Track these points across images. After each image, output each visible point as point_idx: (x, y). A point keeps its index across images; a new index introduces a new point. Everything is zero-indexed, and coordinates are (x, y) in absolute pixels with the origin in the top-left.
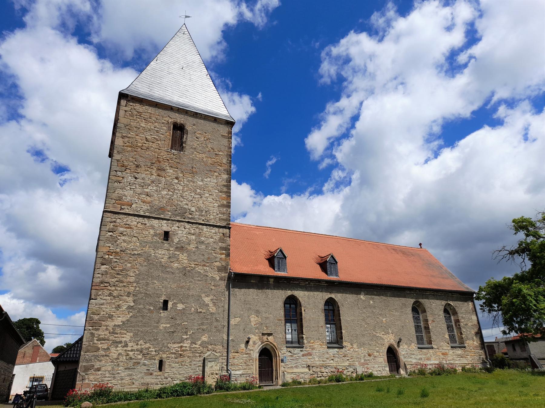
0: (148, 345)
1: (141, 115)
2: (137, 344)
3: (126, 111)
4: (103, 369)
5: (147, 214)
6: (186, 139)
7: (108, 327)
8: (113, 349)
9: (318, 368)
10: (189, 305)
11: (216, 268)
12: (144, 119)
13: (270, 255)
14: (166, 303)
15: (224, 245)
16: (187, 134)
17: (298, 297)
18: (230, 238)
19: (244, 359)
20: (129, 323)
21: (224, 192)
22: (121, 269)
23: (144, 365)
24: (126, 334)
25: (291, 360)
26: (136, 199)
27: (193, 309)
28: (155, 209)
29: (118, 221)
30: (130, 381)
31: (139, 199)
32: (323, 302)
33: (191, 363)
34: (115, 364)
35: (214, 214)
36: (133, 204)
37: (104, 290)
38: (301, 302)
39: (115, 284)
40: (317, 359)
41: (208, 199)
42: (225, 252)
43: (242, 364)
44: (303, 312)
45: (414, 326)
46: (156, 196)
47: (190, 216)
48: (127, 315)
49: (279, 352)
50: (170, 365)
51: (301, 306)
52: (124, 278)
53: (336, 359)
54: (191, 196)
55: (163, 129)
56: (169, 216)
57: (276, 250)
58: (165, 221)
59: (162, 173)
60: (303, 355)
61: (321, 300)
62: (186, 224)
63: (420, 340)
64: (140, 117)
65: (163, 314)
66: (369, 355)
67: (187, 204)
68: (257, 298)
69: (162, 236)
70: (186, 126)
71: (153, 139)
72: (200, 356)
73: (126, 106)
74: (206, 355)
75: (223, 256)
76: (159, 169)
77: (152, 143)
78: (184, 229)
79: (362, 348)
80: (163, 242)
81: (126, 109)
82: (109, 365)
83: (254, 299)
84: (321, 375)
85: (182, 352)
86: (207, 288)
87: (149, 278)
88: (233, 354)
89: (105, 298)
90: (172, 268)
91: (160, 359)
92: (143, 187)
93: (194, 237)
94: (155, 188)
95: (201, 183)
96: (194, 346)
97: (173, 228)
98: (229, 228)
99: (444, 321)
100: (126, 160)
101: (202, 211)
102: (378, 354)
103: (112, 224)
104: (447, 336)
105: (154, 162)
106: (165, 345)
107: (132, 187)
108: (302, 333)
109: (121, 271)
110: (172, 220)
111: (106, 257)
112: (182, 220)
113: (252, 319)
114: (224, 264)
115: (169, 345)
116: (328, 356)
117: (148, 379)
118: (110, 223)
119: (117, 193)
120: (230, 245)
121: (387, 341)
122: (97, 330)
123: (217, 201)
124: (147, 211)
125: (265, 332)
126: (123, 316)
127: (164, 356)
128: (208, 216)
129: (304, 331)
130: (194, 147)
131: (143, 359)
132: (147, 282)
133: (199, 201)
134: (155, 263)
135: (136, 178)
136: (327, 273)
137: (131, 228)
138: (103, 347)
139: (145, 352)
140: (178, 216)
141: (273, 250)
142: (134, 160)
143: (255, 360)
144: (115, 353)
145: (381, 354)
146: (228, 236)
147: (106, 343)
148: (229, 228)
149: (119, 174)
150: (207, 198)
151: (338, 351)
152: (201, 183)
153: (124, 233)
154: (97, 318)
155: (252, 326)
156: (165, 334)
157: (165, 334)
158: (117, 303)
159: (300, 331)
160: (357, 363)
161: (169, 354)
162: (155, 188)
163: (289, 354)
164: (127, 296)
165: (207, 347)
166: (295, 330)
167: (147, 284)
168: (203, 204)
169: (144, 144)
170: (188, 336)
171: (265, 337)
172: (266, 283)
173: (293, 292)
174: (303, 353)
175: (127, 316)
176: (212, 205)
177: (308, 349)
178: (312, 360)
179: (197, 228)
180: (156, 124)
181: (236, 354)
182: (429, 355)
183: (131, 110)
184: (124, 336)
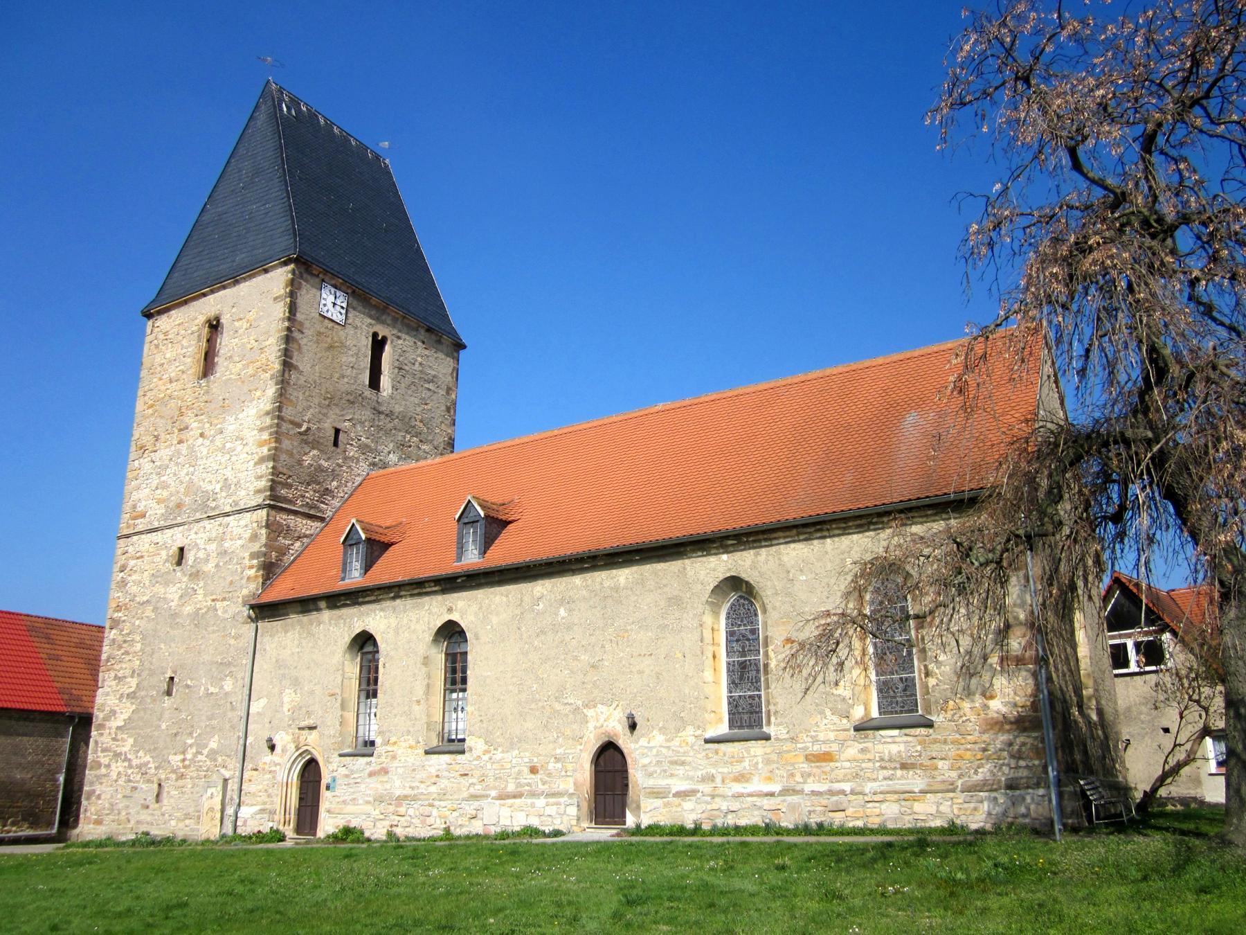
60: (371, 774)
66: (533, 770)
102: (559, 765)
181: (255, 773)
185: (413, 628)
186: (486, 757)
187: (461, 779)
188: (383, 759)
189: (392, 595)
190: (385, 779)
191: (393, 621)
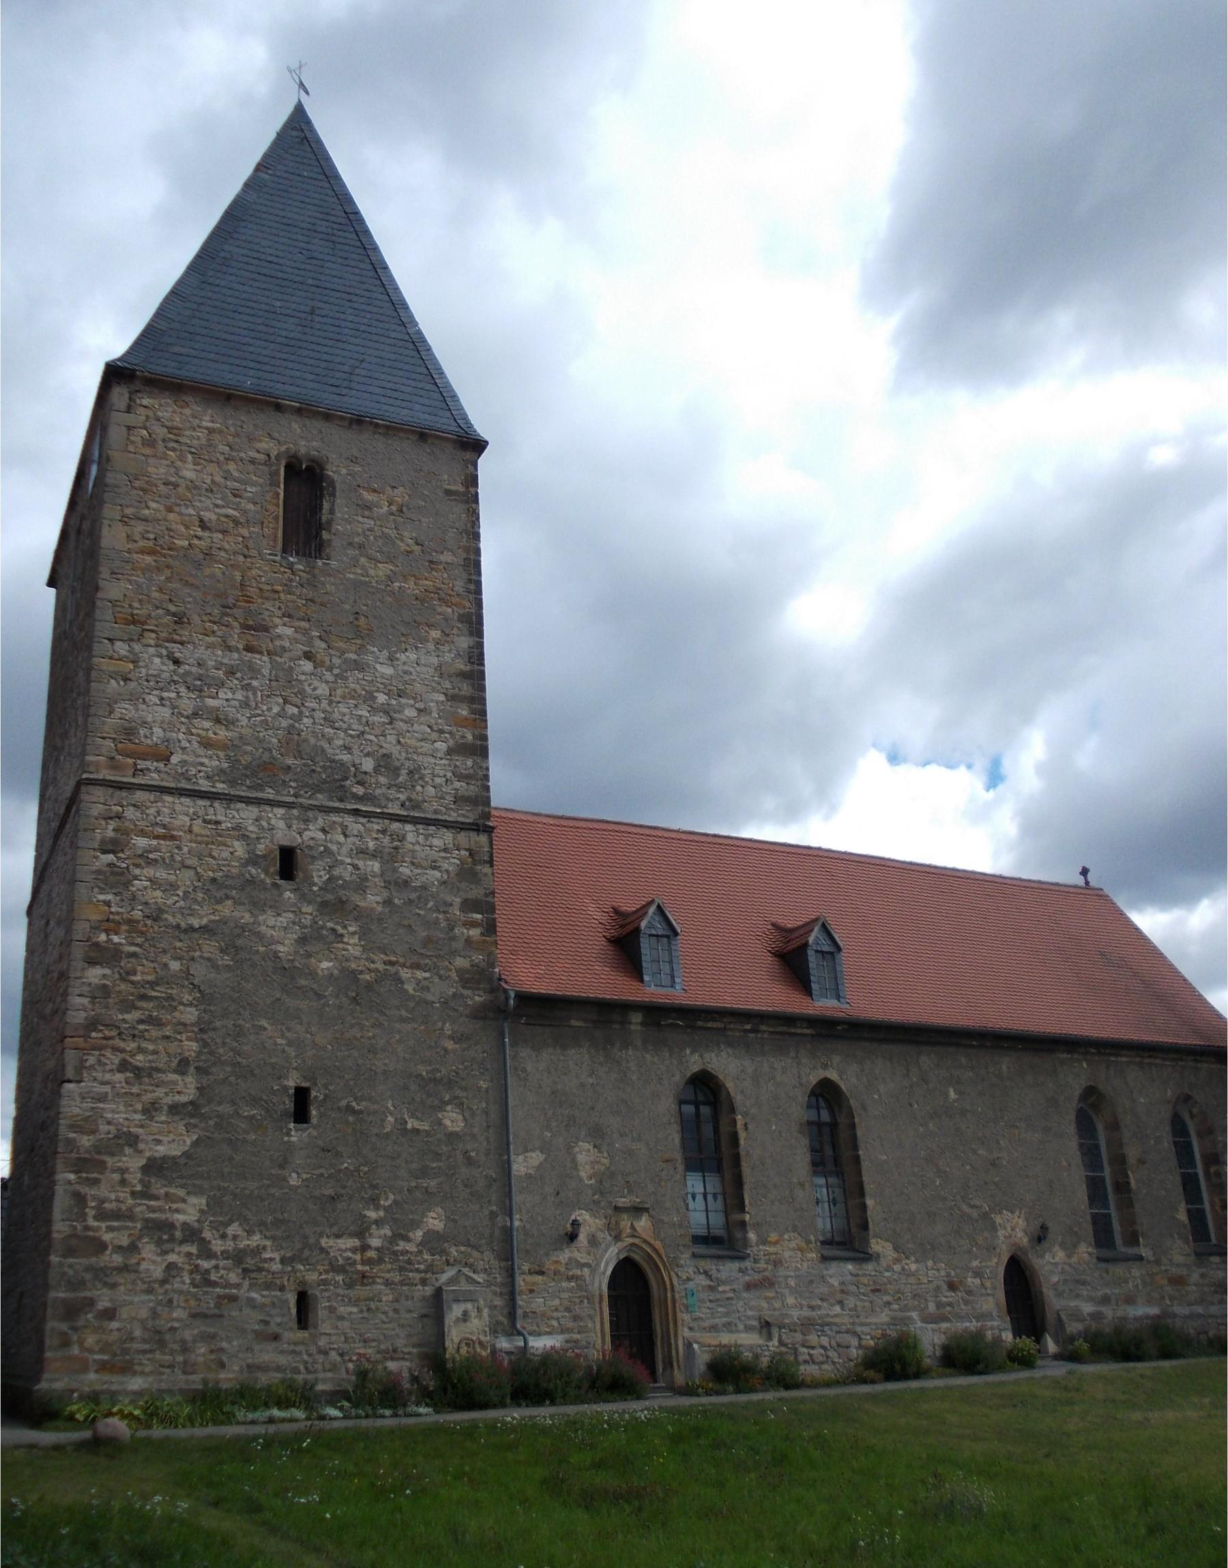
0: (256, 1240)
1: (181, 439)
2: (223, 1236)
3: (129, 428)
4: (124, 1313)
5: (220, 787)
6: (332, 512)
7: (126, 1176)
8: (148, 1250)
9: (795, 1331)
10: (376, 1107)
11: (454, 975)
12: (191, 453)
13: (622, 926)
14: (302, 1096)
15: (476, 892)
16: (333, 495)
17: (721, 1077)
18: (492, 866)
19: (563, 1295)
20: (191, 1163)
21: (465, 697)
22: (149, 978)
23: (251, 1303)
24: (184, 1201)
25: (710, 1301)
26: (181, 736)
27: (390, 1119)
28: (246, 768)
29: (130, 813)
30: (213, 1357)
31: (192, 734)
32: (802, 1097)
33: (396, 1305)
34: (160, 1298)
35: (438, 780)
36: (172, 753)
37: (103, 1052)
38: (732, 1094)
39: (136, 1032)
40: (790, 1300)
41: (416, 727)
42: (479, 916)
43: (560, 1314)
44: (742, 1135)
45: (1084, 1179)
46: (244, 722)
47: (359, 790)
48: (182, 1135)
49: (672, 1273)
50: (332, 1310)
51: (732, 1110)
52: (163, 1012)
53: (851, 1302)
54: (360, 716)
55: (253, 484)
56: (292, 792)
57: (644, 907)
58: (280, 811)
59: (264, 642)
60: (749, 1287)
61: (794, 1087)
62: (349, 820)
63: (1103, 1236)
64: (175, 445)
65: (296, 1135)
66: (952, 1287)
67: (347, 748)
68: (591, 1081)
69: (275, 865)
70: (328, 467)
71: (223, 519)
72: (424, 1282)
73: (129, 410)
74: (444, 1278)
75: (475, 933)
76: (249, 627)
77: (220, 536)
78: (341, 838)
79: (930, 1263)
80: (275, 885)
81: (131, 419)
82: (143, 1302)
83: (582, 1085)
84: (807, 1358)
85: (367, 1268)
86: (430, 1047)
87: (242, 1012)
88: (529, 1278)
89: (108, 1076)
90: (312, 974)
91: (300, 1289)
92: (201, 691)
93: (376, 866)
94: (240, 695)
95: (388, 671)
96: (402, 1245)
97: (307, 833)
98: (489, 830)
99: (1174, 1162)
100: (140, 601)
101: (396, 771)
102: (977, 1281)
103: (112, 825)
104: (1182, 1216)
105: (231, 601)
106: (312, 1241)
107: (165, 694)
108: (741, 1208)
109: (153, 985)
110: (302, 806)
111: (100, 939)
112: (331, 804)
113: (581, 1158)
114: (479, 958)
115: (324, 1242)
116: (824, 1289)
117: (267, 1354)
118: (103, 822)
119: (119, 715)
120: (493, 893)
121: (1005, 1237)
122: (96, 1182)
123: (441, 732)
124: (218, 775)
125: (622, 1202)
126: (170, 1139)
127: (312, 1277)
128: (419, 788)
129: (747, 1202)
130: (356, 540)
131: (246, 1283)
132: (240, 1026)
133: (384, 736)
134: (256, 958)
135: (177, 662)
136: (807, 989)
137: (173, 838)
138: (116, 1242)
139: (250, 1262)
140: (319, 791)
141: (629, 907)
142: (167, 597)
143: (597, 1300)
144: (154, 1262)
145: (988, 1284)
146: (486, 858)
147: (127, 1228)
148: (489, 830)
149: (121, 648)
150: (409, 721)
151: (854, 1272)
152: (388, 671)
153: (151, 856)
154: (87, 1144)
155: (581, 1180)
156: (311, 1206)
157: (311, 1206)
158: (149, 1096)
159: (734, 1197)
160: (914, 1315)
161: (327, 1272)
162: (240, 695)
163: (703, 1283)
164: (175, 1071)
165: (443, 1252)
166: (715, 1198)
167: (239, 1033)
168: (398, 747)
169: (196, 541)
170: (381, 1213)
171: (625, 1222)
172: (617, 1027)
173: (707, 1056)
174: (747, 1278)
175: (185, 1142)
176: (426, 747)
177: (762, 1265)
178: (777, 1305)
179: (384, 832)
180: (232, 467)
181: (539, 1278)
182: (1131, 1285)
183: (148, 424)
184: (180, 1205)
185: (778, 1079)
186: (897, 1267)
187: (873, 1297)
188: (762, 1265)
189: (748, 1027)
190: (771, 1295)
191: (749, 1065)
